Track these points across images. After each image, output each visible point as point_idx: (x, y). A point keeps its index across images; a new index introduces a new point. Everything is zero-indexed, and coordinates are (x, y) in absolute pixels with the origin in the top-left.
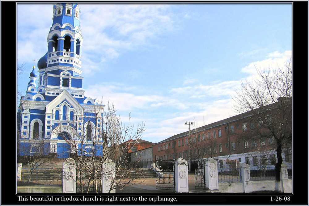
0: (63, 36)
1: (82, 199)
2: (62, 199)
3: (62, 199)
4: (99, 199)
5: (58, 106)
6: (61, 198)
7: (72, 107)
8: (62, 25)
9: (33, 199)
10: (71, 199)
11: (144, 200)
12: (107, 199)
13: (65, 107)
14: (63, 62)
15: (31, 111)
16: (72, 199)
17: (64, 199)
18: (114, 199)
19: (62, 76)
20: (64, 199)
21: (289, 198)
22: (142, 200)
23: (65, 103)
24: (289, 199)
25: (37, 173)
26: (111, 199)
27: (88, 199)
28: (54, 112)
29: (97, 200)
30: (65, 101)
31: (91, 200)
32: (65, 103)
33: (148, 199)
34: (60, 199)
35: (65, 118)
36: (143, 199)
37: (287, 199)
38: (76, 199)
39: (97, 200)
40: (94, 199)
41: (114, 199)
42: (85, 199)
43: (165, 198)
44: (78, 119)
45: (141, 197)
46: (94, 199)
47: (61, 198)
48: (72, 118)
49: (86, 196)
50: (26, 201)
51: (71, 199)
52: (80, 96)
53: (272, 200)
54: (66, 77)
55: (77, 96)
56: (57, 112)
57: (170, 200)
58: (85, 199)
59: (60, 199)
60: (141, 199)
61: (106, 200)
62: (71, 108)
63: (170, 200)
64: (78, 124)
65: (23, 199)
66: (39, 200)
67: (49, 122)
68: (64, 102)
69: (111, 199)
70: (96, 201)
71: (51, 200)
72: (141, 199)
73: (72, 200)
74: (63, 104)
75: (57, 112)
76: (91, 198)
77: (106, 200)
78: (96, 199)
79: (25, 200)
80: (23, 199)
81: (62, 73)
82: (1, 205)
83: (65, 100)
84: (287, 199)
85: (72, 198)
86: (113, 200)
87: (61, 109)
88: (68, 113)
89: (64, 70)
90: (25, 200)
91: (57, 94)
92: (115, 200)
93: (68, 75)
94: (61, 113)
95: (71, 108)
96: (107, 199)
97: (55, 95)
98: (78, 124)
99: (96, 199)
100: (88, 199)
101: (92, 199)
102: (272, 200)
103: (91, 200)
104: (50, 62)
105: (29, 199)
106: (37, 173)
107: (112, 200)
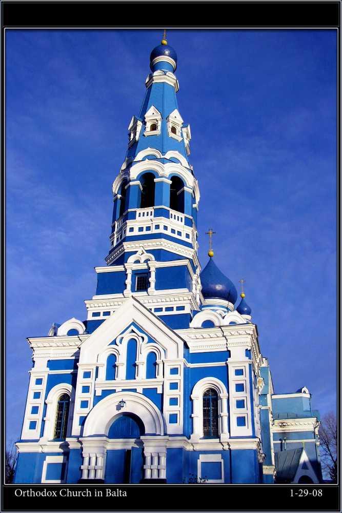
0: (168, 176)
1: (84, 494)
2: (29, 494)
3: (29, 494)
4: (93, 494)
5: (114, 342)
6: (28, 491)
7: (151, 340)
8: (163, 153)
9: (303, 491)
10: (44, 494)
13: (133, 345)
14: (168, 233)
15: (52, 364)
16: (46, 495)
17: (33, 493)
19: (131, 265)
20: (33, 493)
21: (320, 491)
23: (133, 331)
24: (320, 494)
25: (310, 491)
27: (75, 494)
28: (103, 361)
29: (102, 496)
30: (132, 327)
32: (133, 331)
34: (26, 494)
35: (131, 373)
37: (318, 493)
38: (53, 494)
39: (102, 496)
42: (69, 493)
44: (167, 371)
45: (30, 490)
47: (28, 491)
48: (152, 372)
49: (72, 489)
51: (44, 494)
52: (179, 308)
54: (143, 266)
55: (171, 309)
56: (112, 359)
59: (26, 494)
62: (148, 343)
64: (167, 386)
65: (69, 493)
67: (86, 389)
68: (130, 330)
70: (89, 497)
73: (45, 495)
74: (128, 337)
75: (112, 359)
76: (79, 492)
78: (89, 493)
80: (69, 493)
81: (132, 259)
83: (134, 324)
84: (318, 493)
85: (45, 491)
87: (123, 349)
88: (142, 359)
89: (135, 252)
91: (107, 314)
93: (146, 261)
94: (122, 361)
95: (148, 343)
97: (101, 317)
98: (167, 386)
99: (89, 493)
100: (75, 494)
101: (81, 494)
103: (79, 496)
104: (132, 230)
105: (104, 493)
106: (310, 491)
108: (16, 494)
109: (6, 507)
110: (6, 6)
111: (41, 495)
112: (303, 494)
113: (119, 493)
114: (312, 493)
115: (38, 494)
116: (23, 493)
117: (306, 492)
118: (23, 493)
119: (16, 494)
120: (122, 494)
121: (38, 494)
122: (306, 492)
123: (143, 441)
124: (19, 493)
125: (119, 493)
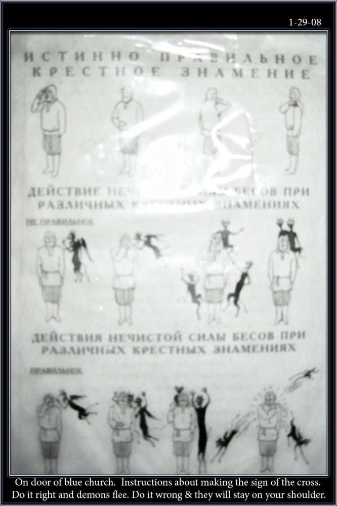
11: (243, 485)
12: (39, 496)
18: (50, 495)
20: (287, 483)
21: (319, 20)
22: (286, 485)
24: (319, 24)
26: (45, 495)
27: (97, 483)
29: (267, 485)
31: (101, 485)
33: (296, 483)
36: (200, 495)
37: (317, 22)
39: (27, 485)
40: (107, 483)
41: (50, 495)
42: (92, 483)
43: (64, 494)
46: (107, 483)
50: (106, 498)
53: (291, 25)
57: (257, 484)
58: (92, 483)
60: (197, 496)
61: (37, 497)
63: (257, 484)
66: (179, 484)
69: (45, 495)
71: (228, 496)
72: (197, 496)
77: (37, 497)
78: (111, 483)
79: (129, 485)
82: (2, 504)
84: (317, 22)
86: (264, 485)
90: (129, 485)
92: (93, 485)
96: (39, 496)
99: (111, 483)
101: (103, 483)
102: (291, 25)
103: (101, 485)
107: (47, 496)
108: (16, 483)
109: (331, 6)
110: (6, 6)
111: (42, 484)
112: (302, 23)
113: (150, 495)
114: (311, 22)
115: (98, 496)
116: (23, 482)
117: (305, 21)
118: (23, 482)
119: (16, 483)
120: (239, 496)
121: (98, 496)
122: (305, 21)
123: (71, 249)
124: (19, 482)
125: (150, 495)
